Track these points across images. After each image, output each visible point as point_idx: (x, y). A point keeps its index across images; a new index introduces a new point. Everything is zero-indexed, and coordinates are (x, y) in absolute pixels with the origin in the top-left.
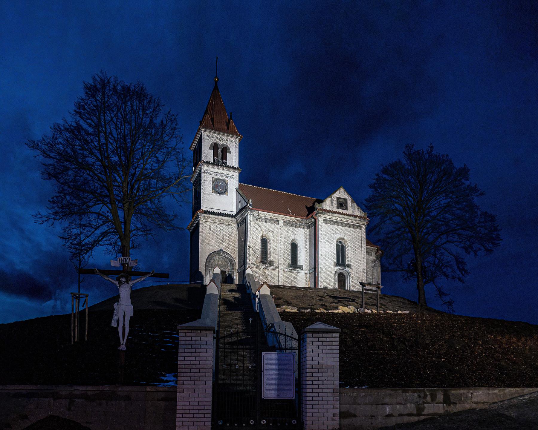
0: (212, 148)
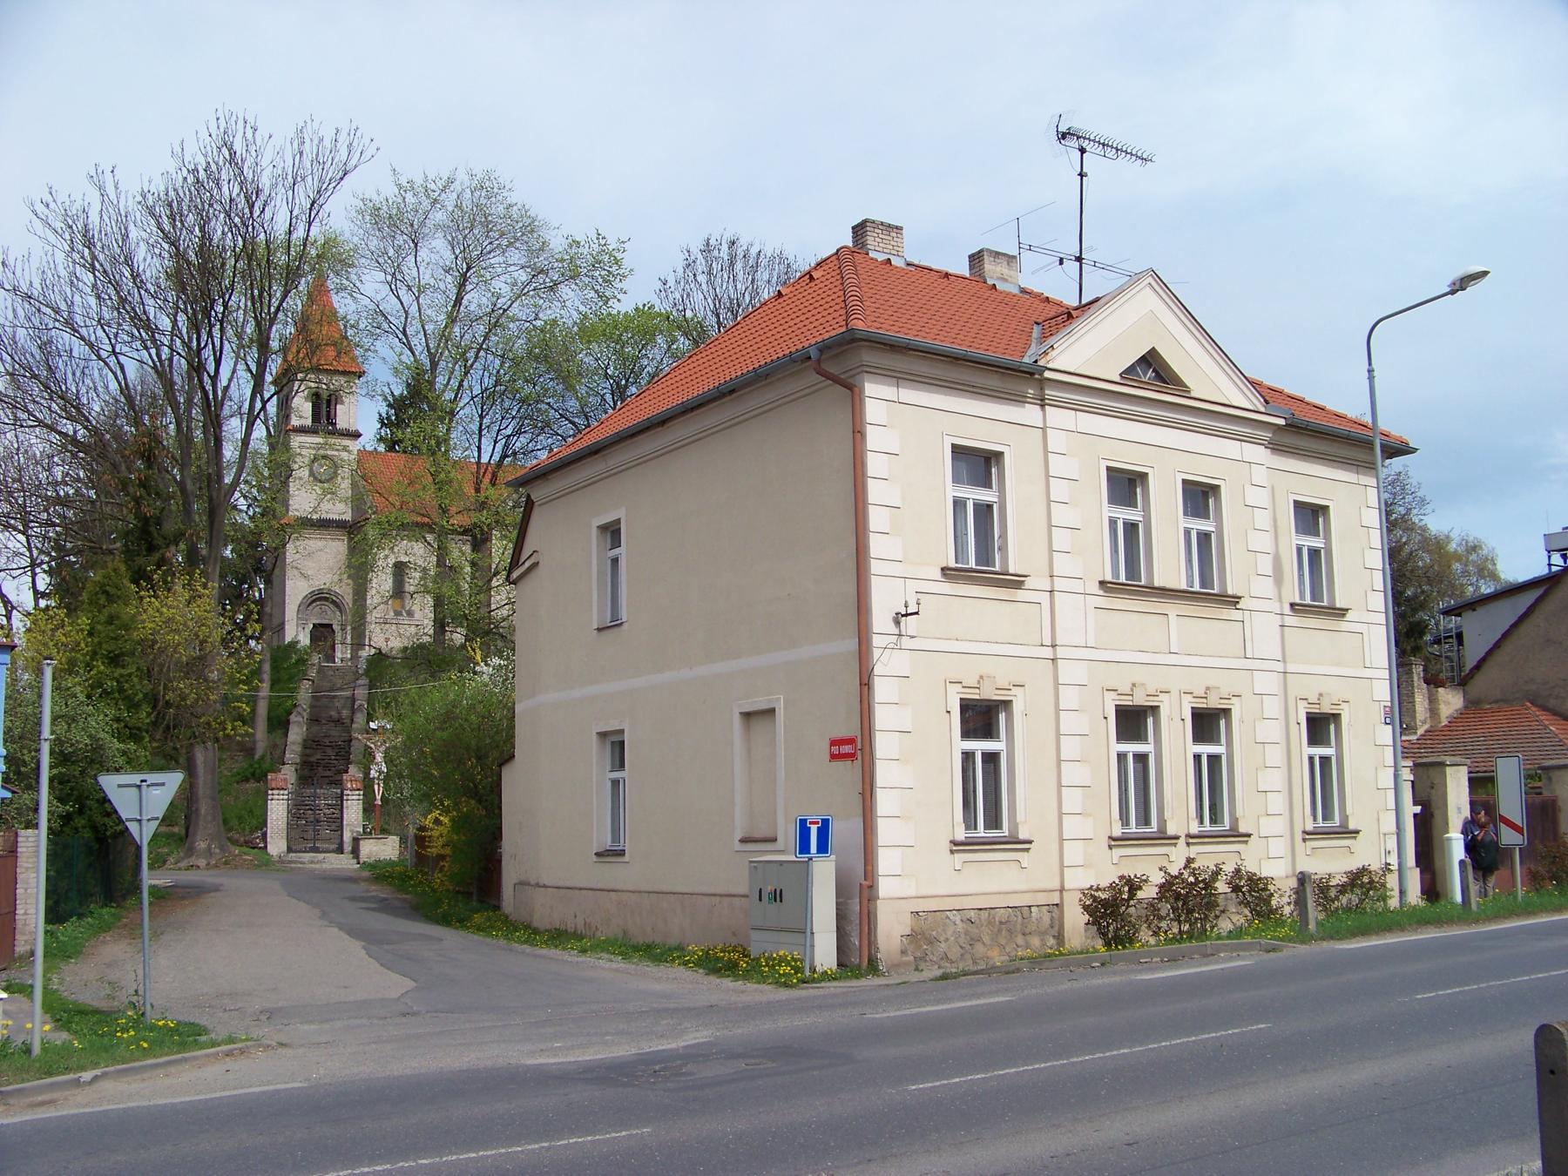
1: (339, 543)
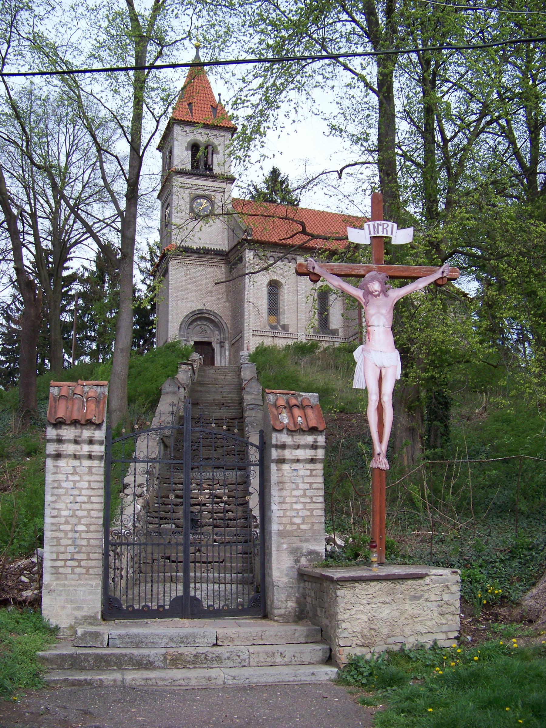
0: (190, 148)
1: (218, 270)
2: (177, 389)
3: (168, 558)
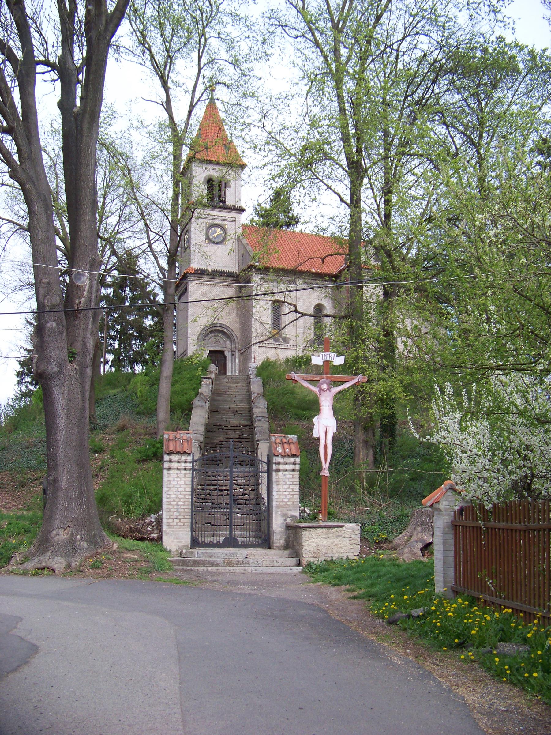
2: (204, 404)
3: (210, 523)
